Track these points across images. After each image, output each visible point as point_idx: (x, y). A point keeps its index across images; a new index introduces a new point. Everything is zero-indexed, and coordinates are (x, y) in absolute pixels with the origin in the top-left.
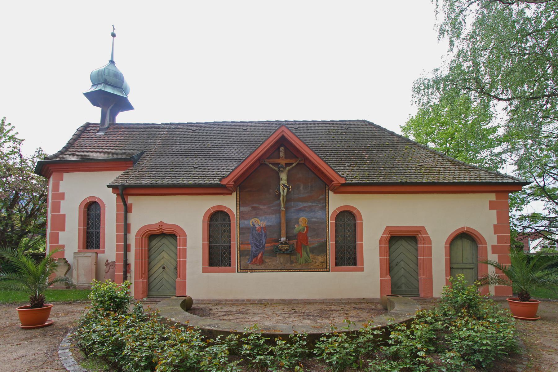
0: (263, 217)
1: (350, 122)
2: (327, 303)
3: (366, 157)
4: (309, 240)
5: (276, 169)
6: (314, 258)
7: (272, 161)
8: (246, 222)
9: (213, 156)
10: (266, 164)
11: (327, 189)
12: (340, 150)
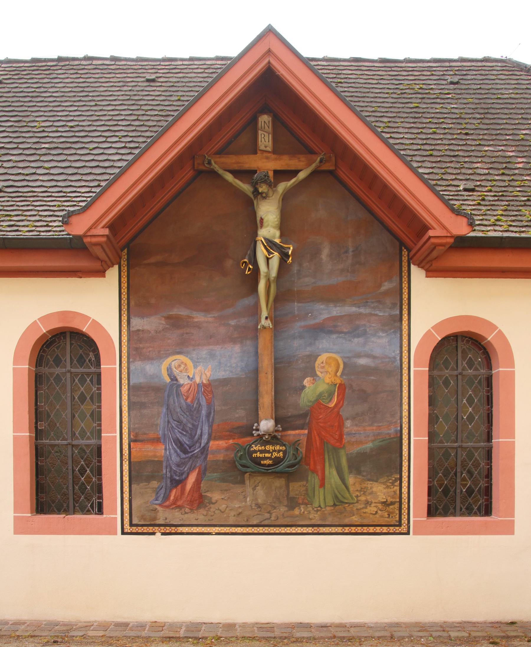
0: (204, 352)
1: (464, 64)
2: (403, 638)
3: (521, 166)
4: (346, 430)
5: (246, 188)
6: (363, 490)
7: (232, 161)
8: (150, 368)
9: (51, 158)
10: (213, 174)
11: (405, 259)
12: (439, 142)
